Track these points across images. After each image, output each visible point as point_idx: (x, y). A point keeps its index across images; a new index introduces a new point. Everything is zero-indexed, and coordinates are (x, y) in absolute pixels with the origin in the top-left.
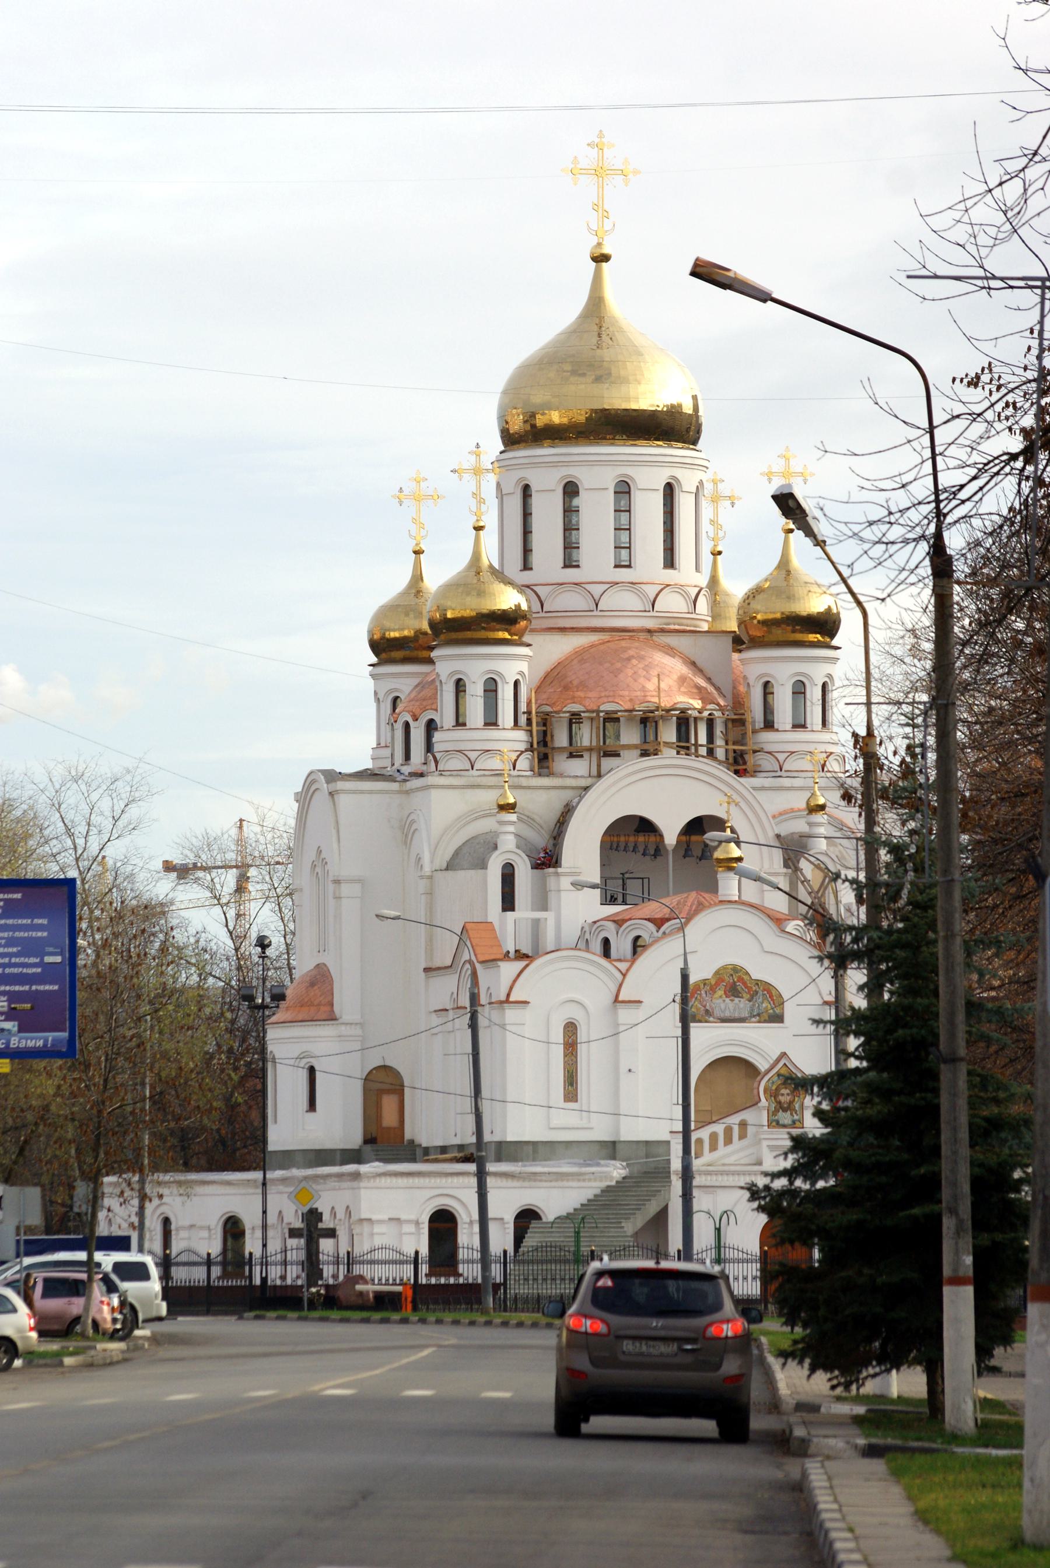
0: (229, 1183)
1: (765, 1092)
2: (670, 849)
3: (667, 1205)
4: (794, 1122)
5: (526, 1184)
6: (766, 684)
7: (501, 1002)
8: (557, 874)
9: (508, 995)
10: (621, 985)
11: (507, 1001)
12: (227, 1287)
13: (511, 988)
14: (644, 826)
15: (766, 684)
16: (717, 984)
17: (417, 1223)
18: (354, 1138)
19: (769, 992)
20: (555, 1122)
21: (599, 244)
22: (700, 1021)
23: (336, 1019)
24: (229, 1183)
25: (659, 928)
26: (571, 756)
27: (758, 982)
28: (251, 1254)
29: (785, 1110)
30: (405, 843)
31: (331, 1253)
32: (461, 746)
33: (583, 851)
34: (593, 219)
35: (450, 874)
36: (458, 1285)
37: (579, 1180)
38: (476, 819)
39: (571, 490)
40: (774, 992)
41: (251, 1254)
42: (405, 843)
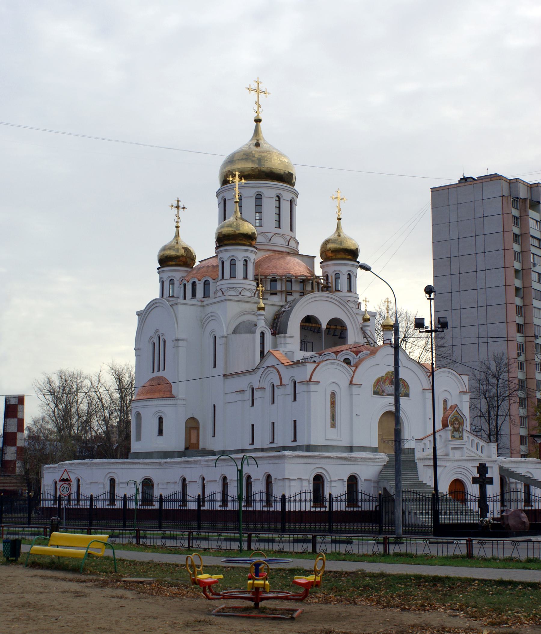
0: (146, 464)
2: (323, 330)
4: (460, 437)
5: (353, 463)
7: (307, 382)
8: (285, 337)
9: (310, 378)
10: (353, 377)
12: (147, 509)
13: (311, 375)
16: (386, 379)
17: (309, 481)
18: (182, 448)
19: (404, 384)
20: (328, 437)
21: (257, 116)
22: (380, 395)
23: (174, 397)
24: (146, 464)
25: (357, 355)
26: (272, 294)
28: (330, 495)
30: (202, 327)
31: (377, 497)
32: (235, 286)
34: (256, 107)
35: (237, 336)
36: (251, 511)
37: (373, 462)
38: (243, 314)
41: (330, 495)
42: (202, 327)
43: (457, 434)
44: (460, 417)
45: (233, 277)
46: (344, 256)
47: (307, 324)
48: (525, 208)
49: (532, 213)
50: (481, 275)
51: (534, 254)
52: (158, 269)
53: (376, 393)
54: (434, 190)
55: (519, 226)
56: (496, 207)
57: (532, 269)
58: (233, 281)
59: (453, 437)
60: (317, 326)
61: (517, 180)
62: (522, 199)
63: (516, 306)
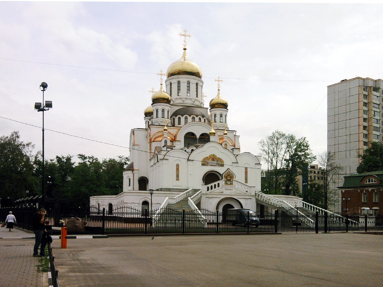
1: (224, 176)
2: (198, 139)
3: (200, 201)
4: (231, 184)
6: (215, 115)
11: (163, 159)
14: (193, 134)
15: (215, 115)
19: (221, 160)
27: (218, 158)
29: (229, 181)
33: (181, 137)
34: (184, 43)
39: (179, 83)
40: (222, 160)
43: (229, 183)
44: (231, 174)
45: (157, 117)
46: (222, 107)
47: (192, 136)
48: (371, 91)
49: (374, 93)
50: (348, 121)
51: (374, 111)
52: (144, 118)
53: (203, 165)
54: (329, 87)
55: (368, 99)
56: (355, 91)
57: (373, 117)
58: (157, 119)
59: (226, 183)
60: (194, 137)
61: (368, 79)
62: (369, 88)
63: (364, 134)
